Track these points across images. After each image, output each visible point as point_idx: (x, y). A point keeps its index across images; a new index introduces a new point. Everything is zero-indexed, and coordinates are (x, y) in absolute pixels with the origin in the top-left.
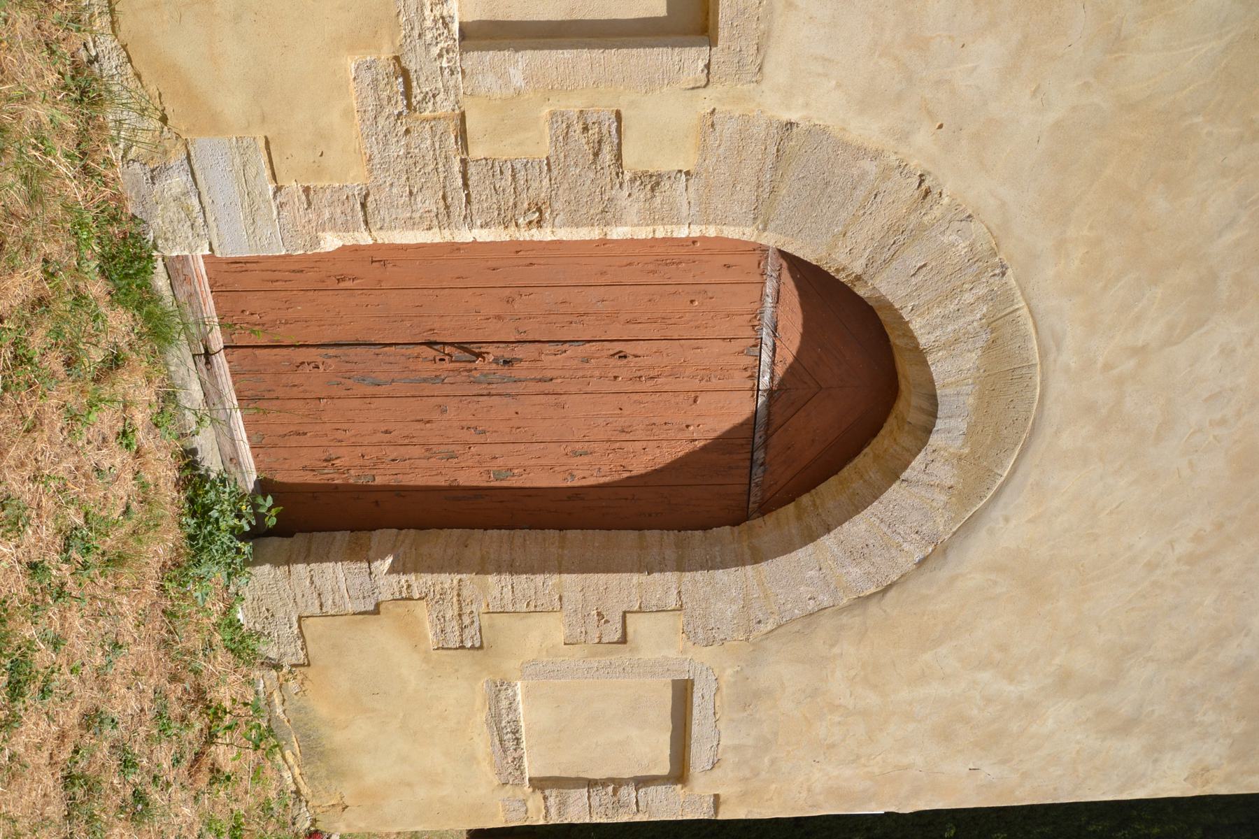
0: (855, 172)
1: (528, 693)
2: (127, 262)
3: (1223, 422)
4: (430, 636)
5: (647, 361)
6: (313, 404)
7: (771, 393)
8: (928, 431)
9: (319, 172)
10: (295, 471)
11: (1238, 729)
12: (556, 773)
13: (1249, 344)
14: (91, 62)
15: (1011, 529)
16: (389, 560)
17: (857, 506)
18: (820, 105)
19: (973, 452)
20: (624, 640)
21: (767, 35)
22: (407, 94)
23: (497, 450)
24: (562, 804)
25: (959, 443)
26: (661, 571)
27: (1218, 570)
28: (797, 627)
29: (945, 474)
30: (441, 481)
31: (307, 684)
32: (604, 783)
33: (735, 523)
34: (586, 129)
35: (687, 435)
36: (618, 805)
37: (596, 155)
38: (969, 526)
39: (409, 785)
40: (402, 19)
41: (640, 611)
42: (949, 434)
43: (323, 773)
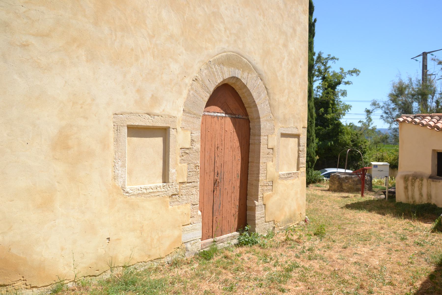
0: (192, 96)
1: (281, 171)
2: (205, 256)
3: (239, 9)
4: (270, 193)
5: (219, 142)
6: (223, 219)
7: (226, 113)
8: (237, 78)
9: (188, 214)
10: (235, 223)
11: (296, 3)
12: (296, 165)
13: (225, 3)
14: (168, 263)
15: (256, 59)
16: (255, 202)
17: (250, 95)
18: (180, 103)
19: (242, 68)
20: (272, 149)
21: (168, 116)
22: (175, 195)
23: (233, 177)
24: (303, 163)
25: (240, 71)
26: (260, 140)
27: (266, 9)
28: (272, 109)
29: (246, 74)
30: (239, 190)
31: (278, 221)
32: (299, 154)
33: (249, 122)
34: (183, 156)
35: (232, 133)
36: (303, 150)
37: (187, 154)
38: (255, 69)
39: (297, 198)
40: (163, 196)
41: (267, 145)
42: (238, 74)
43: (294, 218)
